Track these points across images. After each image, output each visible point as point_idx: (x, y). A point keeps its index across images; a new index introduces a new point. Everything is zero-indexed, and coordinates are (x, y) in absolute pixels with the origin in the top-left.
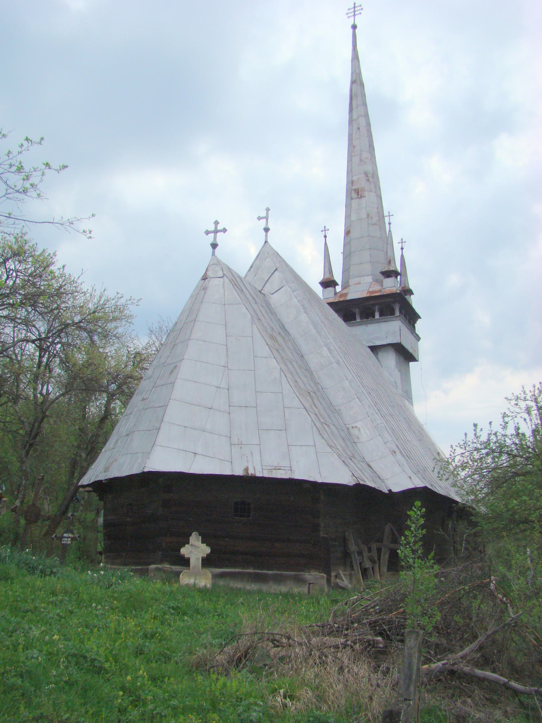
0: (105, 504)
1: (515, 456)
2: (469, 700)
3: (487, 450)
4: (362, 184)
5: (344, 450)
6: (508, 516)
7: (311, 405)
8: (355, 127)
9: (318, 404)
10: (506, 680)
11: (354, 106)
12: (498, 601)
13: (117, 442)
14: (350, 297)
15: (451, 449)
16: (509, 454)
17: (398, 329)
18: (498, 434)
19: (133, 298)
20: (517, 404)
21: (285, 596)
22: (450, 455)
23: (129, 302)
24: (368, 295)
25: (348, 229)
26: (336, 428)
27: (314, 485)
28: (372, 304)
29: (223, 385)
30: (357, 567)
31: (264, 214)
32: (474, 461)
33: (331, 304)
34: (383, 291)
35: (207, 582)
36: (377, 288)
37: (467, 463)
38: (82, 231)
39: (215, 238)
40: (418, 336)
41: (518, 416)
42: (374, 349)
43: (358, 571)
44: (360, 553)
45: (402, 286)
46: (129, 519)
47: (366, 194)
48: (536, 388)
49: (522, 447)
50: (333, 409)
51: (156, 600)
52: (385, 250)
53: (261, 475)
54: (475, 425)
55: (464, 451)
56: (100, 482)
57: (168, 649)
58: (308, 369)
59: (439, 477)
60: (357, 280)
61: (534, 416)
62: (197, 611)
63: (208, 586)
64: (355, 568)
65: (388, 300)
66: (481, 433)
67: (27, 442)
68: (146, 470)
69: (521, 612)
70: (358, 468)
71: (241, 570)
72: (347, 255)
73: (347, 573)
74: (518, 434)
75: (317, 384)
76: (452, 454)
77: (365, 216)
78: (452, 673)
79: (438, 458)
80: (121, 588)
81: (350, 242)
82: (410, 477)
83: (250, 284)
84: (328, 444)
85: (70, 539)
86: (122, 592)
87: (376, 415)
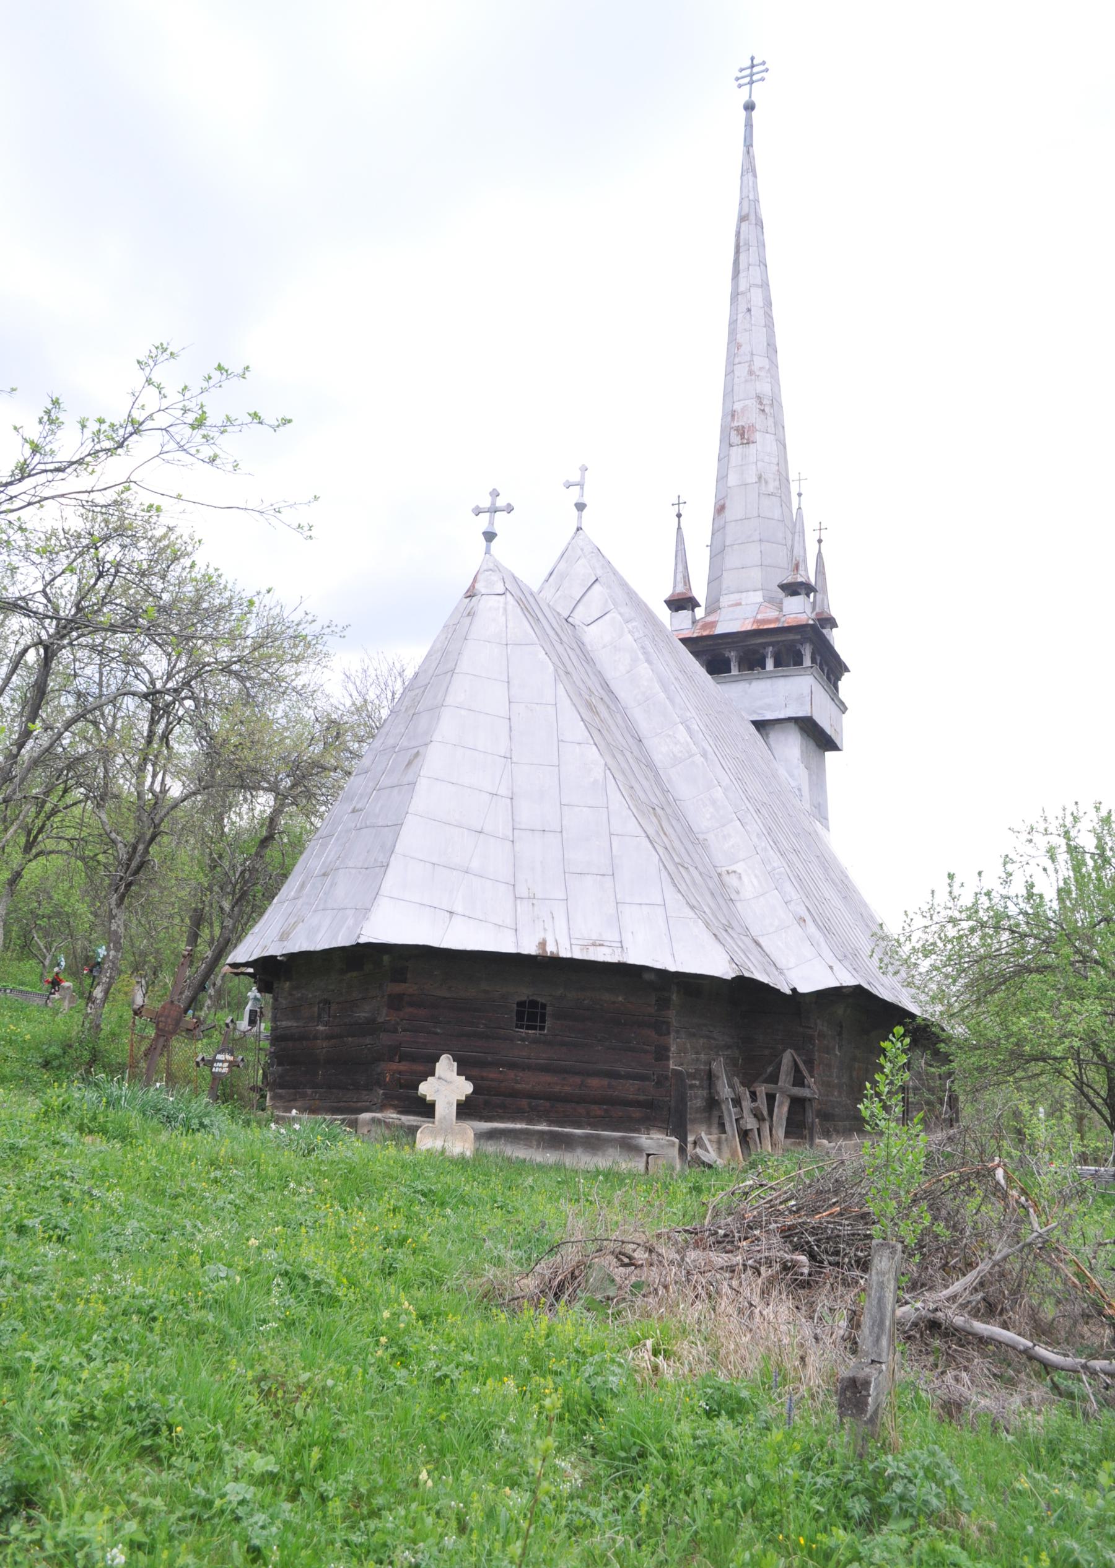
0: (275, 999)
1: (1023, 936)
2: (964, 1374)
3: (971, 923)
4: (751, 417)
5: (713, 914)
6: (1010, 1046)
7: (657, 832)
8: (742, 307)
9: (669, 830)
10: (1030, 1344)
11: (742, 267)
12: (1012, 1203)
13: (303, 886)
14: (720, 630)
15: (905, 918)
16: (1013, 932)
17: (807, 691)
18: (993, 894)
19: (334, 624)
20: (1030, 841)
21: (608, 1175)
22: (904, 929)
23: (326, 631)
24: (755, 627)
25: (722, 502)
26: (700, 874)
27: (663, 974)
28: (761, 644)
29: (503, 791)
30: (731, 1129)
31: (576, 478)
32: (947, 941)
33: (684, 641)
34: (783, 619)
35: (467, 1145)
36: (772, 614)
37: (934, 944)
38: (295, 525)
39: (491, 523)
40: (842, 703)
41: (1033, 862)
42: (761, 726)
43: (734, 1136)
44: (737, 1102)
45: (818, 610)
46: (321, 1028)
47: (758, 436)
48: (1068, 813)
49: (1036, 918)
50: (694, 839)
51: (391, 1177)
52: (789, 543)
53: (569, 956)
54: (951, 876)
55: (930, 922)
56: (273, 958)
57: (435, 1266)
58: (650, 765)
59: (881, 968)
60: (734, 598)
61: (1063, 863)
62: (463, 1200)
63: (468, 1154)
64: (728, 1128)
65: (791, 637)
66: (962, 891)
67: (122, 878)
68: (362, 940)
69: (1054, 1225)
70: (739, 947)
71: (524, 1126)
72: (718, 552)
73: (714, 1137)
74: (1030, 896)
75: (665, 792)
76: (907, 927)
77: (755, 479)
78: (934, 1325)
79: (880, 933)
80: (331, 1155)
81: (724, 527)
82: (831, 967)
83: (549, 606)
84: (688, 903)
85: (226, 1065)
86: (333, 1162)
87: (771, 852)
